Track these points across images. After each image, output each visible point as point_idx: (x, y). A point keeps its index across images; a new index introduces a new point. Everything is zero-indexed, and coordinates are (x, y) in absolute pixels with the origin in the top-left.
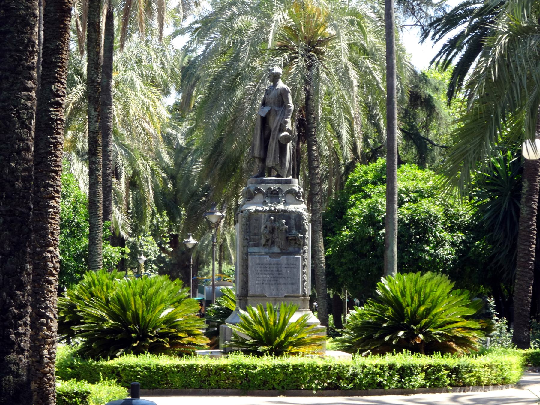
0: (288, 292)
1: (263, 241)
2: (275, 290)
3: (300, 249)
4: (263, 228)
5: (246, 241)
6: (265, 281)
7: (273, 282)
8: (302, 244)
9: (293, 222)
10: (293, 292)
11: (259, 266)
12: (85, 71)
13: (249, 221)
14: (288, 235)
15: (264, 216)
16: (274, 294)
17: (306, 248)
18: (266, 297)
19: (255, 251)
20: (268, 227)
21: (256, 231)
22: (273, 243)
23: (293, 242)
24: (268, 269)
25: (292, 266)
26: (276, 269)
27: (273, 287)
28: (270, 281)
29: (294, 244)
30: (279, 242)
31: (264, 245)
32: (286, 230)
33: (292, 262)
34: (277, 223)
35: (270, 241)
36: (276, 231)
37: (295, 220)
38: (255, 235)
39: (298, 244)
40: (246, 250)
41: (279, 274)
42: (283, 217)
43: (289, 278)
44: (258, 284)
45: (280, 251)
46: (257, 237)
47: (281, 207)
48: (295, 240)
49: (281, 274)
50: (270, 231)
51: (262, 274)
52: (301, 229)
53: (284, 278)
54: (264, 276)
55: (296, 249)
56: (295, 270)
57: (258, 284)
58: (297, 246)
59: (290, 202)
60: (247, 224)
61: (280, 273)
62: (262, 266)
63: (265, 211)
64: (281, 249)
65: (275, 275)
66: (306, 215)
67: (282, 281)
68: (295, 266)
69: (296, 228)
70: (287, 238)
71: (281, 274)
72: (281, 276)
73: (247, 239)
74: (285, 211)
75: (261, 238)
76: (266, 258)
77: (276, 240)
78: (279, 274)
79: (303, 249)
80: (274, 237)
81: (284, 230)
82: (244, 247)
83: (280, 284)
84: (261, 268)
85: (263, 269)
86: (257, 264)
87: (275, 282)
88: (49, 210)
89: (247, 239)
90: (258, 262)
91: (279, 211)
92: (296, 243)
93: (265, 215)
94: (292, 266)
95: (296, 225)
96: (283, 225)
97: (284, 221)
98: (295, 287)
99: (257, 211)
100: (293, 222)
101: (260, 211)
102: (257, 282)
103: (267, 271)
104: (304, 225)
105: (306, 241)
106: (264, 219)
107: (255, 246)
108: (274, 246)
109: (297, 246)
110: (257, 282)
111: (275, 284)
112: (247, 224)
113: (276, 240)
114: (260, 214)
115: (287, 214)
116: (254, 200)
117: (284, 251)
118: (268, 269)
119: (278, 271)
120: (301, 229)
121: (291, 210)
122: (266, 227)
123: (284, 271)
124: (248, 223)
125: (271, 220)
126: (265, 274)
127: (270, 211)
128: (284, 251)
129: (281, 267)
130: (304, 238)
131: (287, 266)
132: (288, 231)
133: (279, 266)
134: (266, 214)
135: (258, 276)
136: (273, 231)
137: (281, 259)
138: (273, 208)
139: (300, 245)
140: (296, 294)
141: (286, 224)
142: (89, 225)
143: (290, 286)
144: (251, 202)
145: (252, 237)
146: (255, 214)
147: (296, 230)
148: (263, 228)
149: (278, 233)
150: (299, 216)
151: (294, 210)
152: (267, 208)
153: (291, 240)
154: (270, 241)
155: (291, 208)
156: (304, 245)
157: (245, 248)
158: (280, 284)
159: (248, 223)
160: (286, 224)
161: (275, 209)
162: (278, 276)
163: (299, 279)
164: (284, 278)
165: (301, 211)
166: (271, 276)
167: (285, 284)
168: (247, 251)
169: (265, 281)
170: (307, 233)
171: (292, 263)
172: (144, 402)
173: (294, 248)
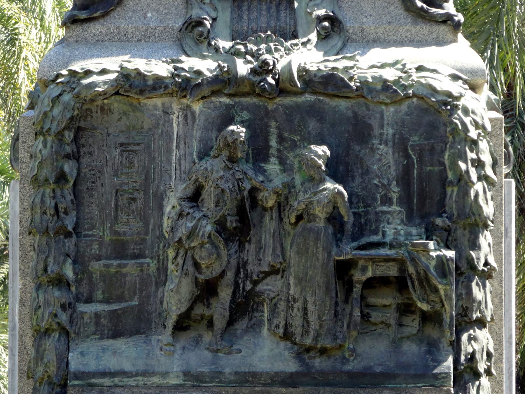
1: (175, 296)
3: (433, 350)
4: (171, 204)
5: (56, 294)
8: (450, 312)
9: (383, 160)
13: (76, 157)
14: (348, 251)
15: (181, 124)
17: (479, 341)
19: (111, 363)
20: (209, 197)
21: (129, 226)
22: (244, 307)
23: (387, 299)
29: (391, 317)
30: (290, 302)
31: (182, 325)
32: (334, 219)
34: (273, 167)
35: (225, 294)
36: (269, 223)
37: (401, 145)
38: (120, 250)
39: (426, 318)
40: (51, 356)
42: (312, 125)
45: (291, 366)
46: (131, 268)
47: (305, 56)
48: (401, 283)
50: (220, 225)
52: (441, 211)
55: (411, 349)
58: (413, 324)
59: (372, 29)
60: (61, 178)
63: (186, 86)
64: (302, 352)
66: (479, 108)
69: (406, 200)
70: (343, 269)
73: (59, 281)
74: (329, 84)
75: (163, 270)
77: (271, 286)
79: (456, 347)
80: (253, 268)
81: (320, 213)
82: (41, 334)
89: (59, 281)
91: (283, 87)
92: (406, 309)
93: (188, 114)
95: (405, 178)
96: (314, 180)
97: (323, 150)
99: (131, 84)
100: (383, 160)
101: (157, 84)
104: (463, 182)
105: (478, 293)
106: (184, 139)
107: (117, 328)
108: (255, 327)
109: (413, 324)
112: (61, 178)
113: (271, 286)
114: (156, 102)
115: (343, 104)
116: (120, 21)
117: (318, 363)
120: (441, 211)
121: (369, 75)
122: (195, 197)
124: (69, 167)
125: (231, 145)
127: (225, 81)
128: (318, 363)
130: (466, 271)
132: (352, 224)
134: (197, 107)
136: (241, 222)
138: (243, 68)
139: (431, 318)
141: (336, 169)
142: (431, 254)
144: (95, 29)
145: (96, 266)
146: (117, 104)
147: (409, 219)
148: (171, 204)
149: (279, 236)
150: (431, 117)
151: (390, 75)
152: (207, 66)
153: (371, 284)
154: (225, 294)
155: (371, 64)
156: (467, 319)
157: (50, 344)
159: (69, 167)
160: (336, 169)
161: (263, 69)
165: (443, 84)
168: (63, 362)
170: (485, 240)
172: (470, 254)
173: (396, 343)
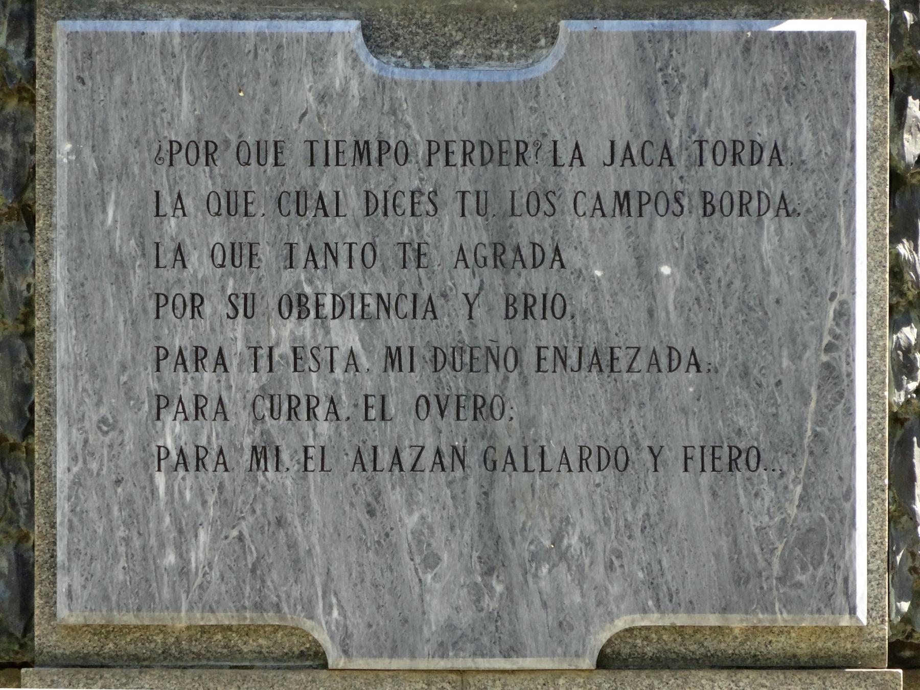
0: (657, 591)
2: (454, 553)
6: (298, 408)
7: (427, 434)
10: (742, 582)
11: (202, 181)
12: (8, 297)
16: (437, 611)
18: (315, 658)
24: (336, 229)
25: (717, 177)
26: (476, 233)
27: (418, 509)
28: (377, 408)
33: (722, 106)
41: (522, 307)
43: (671, 359)
44: (192, 460)
49: (554, 306)
51: (244, 306)
53: (604, 361)
54: (286, 332)
56: (772, 238)
57: (192, 460)
61: (539, 281)
62: (257, 180)
65: (453, 326)
67: (562, 411)
68: (767, 179)
71: (554, 306)
72: (546, 332)
76: (318, 52)
78: (522, 307)
83: (531, 458)
84: (233, 204)
85: (263, 229)
86: (171, 153)
87: (459, 431)
88: (913, 653)
90: (184, 113)
94: (717, 177)
98: (768, 504)
102: (173, 433)
103: (324, 254)
110: (173, 433)
111: (450, 459)
118: (336, 229)
119: (500, 255)
123: (597, 252)
126: (297, 305)
129: (543, 201)
131: (643, 179)
133: (523, 180)
135: (181, 335)
137: (547, 63)
140: (791, 624)
143: (687, 495)
158: (531, 458)
162: (492, 329)
163: (836, 379)
164: (604, 361)
166: (394, 330)
167: (614, 459)
169: (298, 408)
171: (727, 127)
